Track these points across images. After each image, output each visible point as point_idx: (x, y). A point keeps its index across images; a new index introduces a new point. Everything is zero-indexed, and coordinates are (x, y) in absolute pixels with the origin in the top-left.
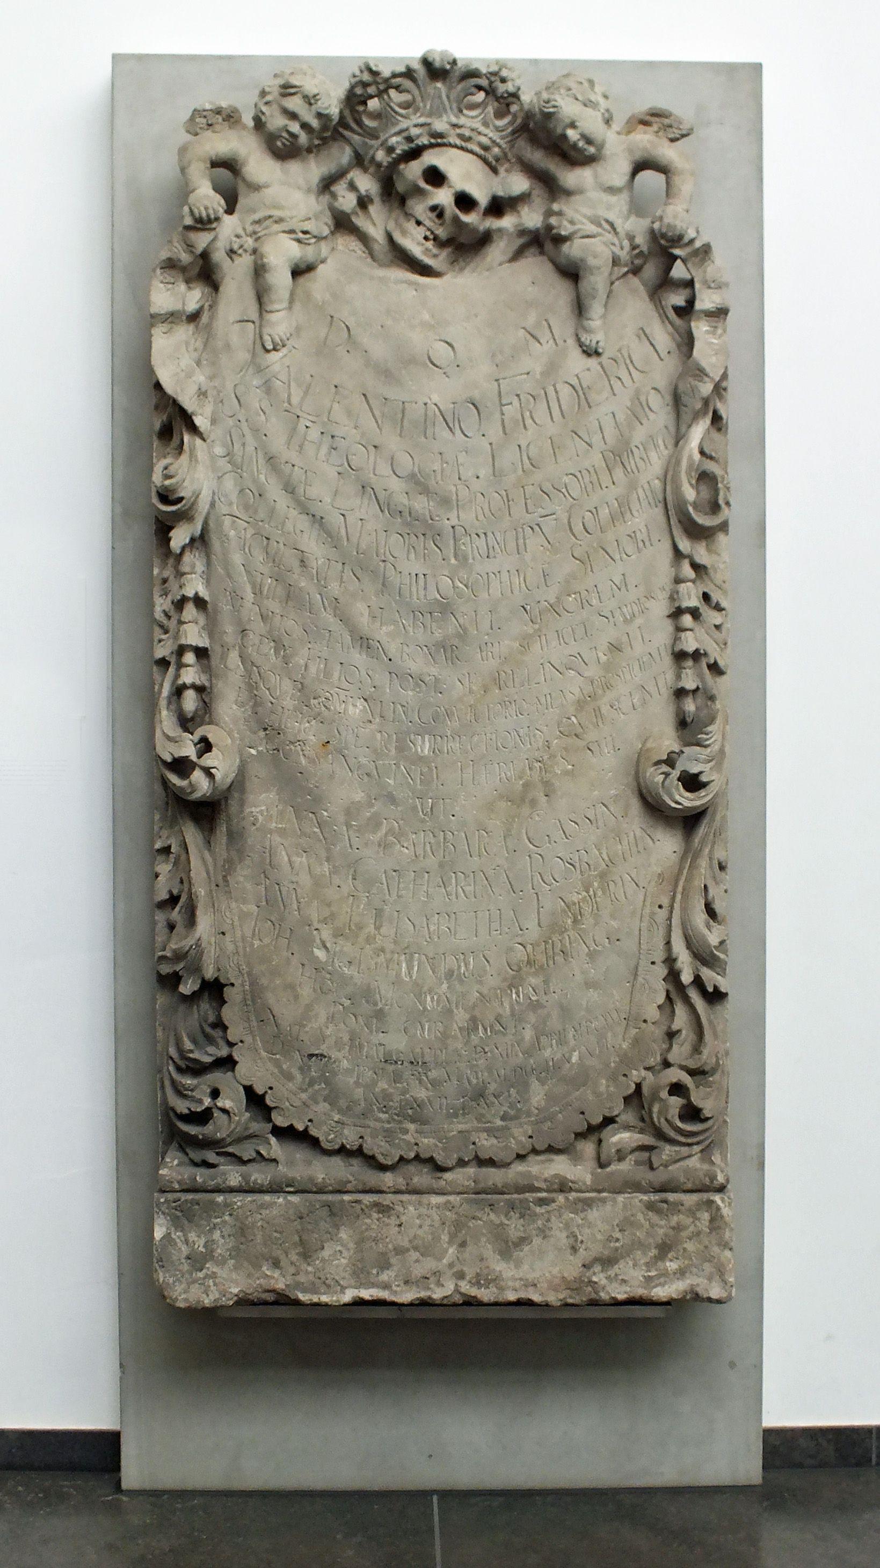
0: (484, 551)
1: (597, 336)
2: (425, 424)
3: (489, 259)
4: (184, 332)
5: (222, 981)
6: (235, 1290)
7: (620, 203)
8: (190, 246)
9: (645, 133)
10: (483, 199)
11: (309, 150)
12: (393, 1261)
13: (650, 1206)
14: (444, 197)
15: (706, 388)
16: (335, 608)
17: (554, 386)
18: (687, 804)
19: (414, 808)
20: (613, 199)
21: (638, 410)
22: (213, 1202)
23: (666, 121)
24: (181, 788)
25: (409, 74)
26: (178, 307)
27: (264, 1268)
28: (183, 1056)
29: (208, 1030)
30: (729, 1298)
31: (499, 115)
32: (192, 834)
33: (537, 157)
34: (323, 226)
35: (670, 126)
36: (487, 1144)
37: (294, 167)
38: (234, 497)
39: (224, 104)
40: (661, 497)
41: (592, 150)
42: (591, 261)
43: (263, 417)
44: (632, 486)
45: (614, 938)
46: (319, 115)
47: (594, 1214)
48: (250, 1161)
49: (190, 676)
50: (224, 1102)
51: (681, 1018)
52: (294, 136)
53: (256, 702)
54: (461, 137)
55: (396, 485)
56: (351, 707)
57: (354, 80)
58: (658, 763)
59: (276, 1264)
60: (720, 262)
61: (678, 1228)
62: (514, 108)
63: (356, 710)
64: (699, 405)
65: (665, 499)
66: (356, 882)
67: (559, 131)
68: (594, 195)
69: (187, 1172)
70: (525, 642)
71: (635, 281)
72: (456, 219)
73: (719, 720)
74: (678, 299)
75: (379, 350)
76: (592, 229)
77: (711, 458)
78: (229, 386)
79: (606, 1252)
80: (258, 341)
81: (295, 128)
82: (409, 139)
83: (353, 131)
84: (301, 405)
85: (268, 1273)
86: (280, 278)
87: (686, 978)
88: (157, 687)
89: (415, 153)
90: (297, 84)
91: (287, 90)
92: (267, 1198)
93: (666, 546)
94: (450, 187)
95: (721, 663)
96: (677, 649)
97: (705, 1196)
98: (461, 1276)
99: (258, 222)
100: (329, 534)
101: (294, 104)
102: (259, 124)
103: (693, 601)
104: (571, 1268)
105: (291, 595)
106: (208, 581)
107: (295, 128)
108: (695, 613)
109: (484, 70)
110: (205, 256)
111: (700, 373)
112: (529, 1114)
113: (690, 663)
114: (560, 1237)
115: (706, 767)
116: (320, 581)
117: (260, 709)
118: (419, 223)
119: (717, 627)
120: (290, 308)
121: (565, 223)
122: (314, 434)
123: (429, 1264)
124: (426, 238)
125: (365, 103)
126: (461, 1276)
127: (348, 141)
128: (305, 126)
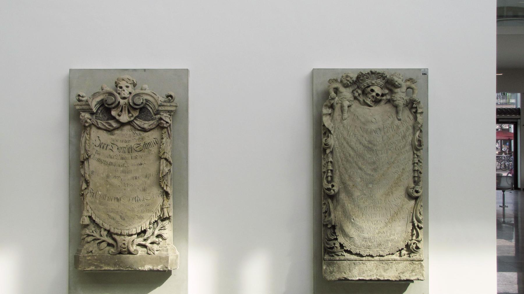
0: (381, 153)
1: (400, 117)
2: (371, 133)
3: (381, 104)
4: (328, 117)
5: (335, 225)
6: (338, 277)
7: (404, 94)
8: (330, 103)
9: (409, 82)
10: (380, 94)
11: (350, 86)
12: (365, 272)
13: (410, 264)
14: (374, 94)
15: (420, 126)
16: (355, 163)
17: (393, 126)
18: (416, 195)
19: (369, 196)
20: (403, 94)
21: (408, 129)
22: (334, 262)
23: (412, 80)
24: (329, 193)
25: (368, 73)
26: (328, 113)
27: (343, 274)
28: (328, 238)
29: (332, 233)
30: (424, 280)
31: (383, 80)
32: (330, 201)
33: (390, 87)
34: (352, 99)
35: (413, 81)
36: (382, 253)
37: (348, 89)
38: (338, 144)
39: (335, 78)
40: (411, 144)
41: (400, 86)
42: (400, 105)
43: (343, 131)
44: (406, 142)
45: (403, 218)
46: (353, 81)
47: (400, 265)
48: (340, 255)
49: (330, 174)
50: (336, 245)
51: (415, 232)
52: (348, 84)
53: (341, 179)
54: (377, 84)
55: (366, 143)
56: (358, 179)
57: (358, 74)
58: (411, 188)
59: (345, 273)
60: (422, 104)
61: (415, 267)
62: (386, 79)
63: (359, 180)
64: (418, 129)
65: (412, 144)
66: (359, 209)
67: (394, 82)
68: (400, 93)
69: (329, 257)
70: (388, 168)
71: (407, 108)
72: (376, 98)
73: (421, 181)
74: (414, 110)
75: (363, 120)
76: (400, 99)
77: (420, 137)
78: (337, 126)
79: (402, 271)
80: (342, 119)
81: (348, 83)
82: (368, 84)
83: (358, 83)
84: (349, 129)
85: (344, 274)
86: (346, 108)
87: (416, 225)
88: (323, 176)
89: (369, 87)
90: (349, 75)
91: (347, 76)
92: (343, 261)
93: (412, 152)
94: (375, 92)
95: (421, 172)
96: (414, 169)
97: (420, 262)
98: (377, 275)
99: (342, 98)
100: (354, 150)
101: (349, 79)
102: (341, 82)
103: (417, 161)
104: (397, 274)
105: (347, 161)
106: (332, 158)
107: (348, 83)
108: (417, 163)
109: (381, 73)
110: (333, 104)
111: (419, 123)
112: (388, 248)
113: (416, 172)
114: (394, 268)
115: (419, 189)
116: (353, 158)
117: (342, 180)
118: (369, 98)
119: (421, 166)
120: (347, 113)
121: (395, 98)
122: (352, 134)
123: (372, 273)
124: (371, 101)
125: (360, 78)
126: (377, 275)
127: (356, 84)
128: (350, 82)
